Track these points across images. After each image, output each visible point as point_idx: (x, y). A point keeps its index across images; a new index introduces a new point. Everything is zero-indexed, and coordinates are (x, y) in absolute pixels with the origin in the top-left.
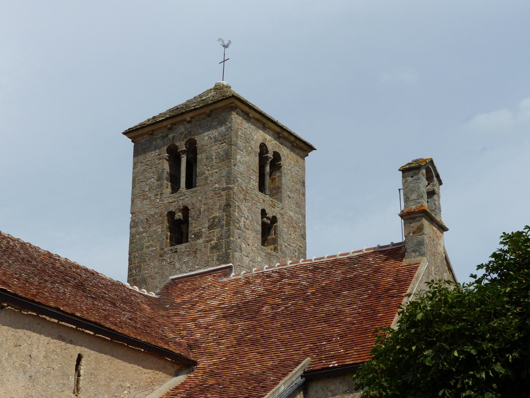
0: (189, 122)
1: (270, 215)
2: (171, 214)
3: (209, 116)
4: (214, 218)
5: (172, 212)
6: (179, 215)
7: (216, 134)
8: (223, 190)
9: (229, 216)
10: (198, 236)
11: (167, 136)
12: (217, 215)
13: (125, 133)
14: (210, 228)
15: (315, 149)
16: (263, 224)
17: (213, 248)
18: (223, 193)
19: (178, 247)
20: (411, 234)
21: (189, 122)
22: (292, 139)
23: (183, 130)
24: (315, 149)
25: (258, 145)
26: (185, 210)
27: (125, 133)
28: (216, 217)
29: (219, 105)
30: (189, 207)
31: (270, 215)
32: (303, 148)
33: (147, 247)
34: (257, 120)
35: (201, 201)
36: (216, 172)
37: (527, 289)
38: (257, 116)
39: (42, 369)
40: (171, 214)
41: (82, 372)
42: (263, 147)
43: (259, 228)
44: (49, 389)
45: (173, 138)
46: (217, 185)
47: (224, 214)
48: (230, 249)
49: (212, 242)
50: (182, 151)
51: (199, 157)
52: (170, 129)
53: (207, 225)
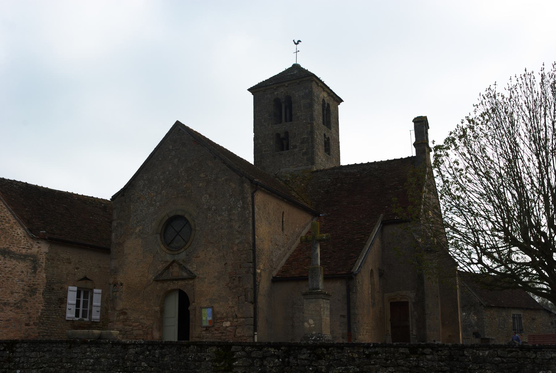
0: (287, 86)
1: (327, 137)
3: (298, 84)
6: (282, 136)
8: (309, 124)
9: (313, 138)
10: (295, 147)
11: (273, 93)
12: (306, 136)
13: (249, 90)
14: (302, 143)
17: (304, 154)
18: (309, 125)
19: (283, 152)
21: (287, 86)
22: (329, 92)
26: (287, 133)
27: (249, 90)
29: (304, 79)
31: (327, 137)
32: (340, 100)
33: (265, 151)
34: (321, 87)
37: (555, 149)
38: (322, 85)
40: (278, 135)
42: (323, 100)
43: (323, 143)
45: (277, 94)
51: (293, 105)
52: (275, 89)
53: (300, 141)
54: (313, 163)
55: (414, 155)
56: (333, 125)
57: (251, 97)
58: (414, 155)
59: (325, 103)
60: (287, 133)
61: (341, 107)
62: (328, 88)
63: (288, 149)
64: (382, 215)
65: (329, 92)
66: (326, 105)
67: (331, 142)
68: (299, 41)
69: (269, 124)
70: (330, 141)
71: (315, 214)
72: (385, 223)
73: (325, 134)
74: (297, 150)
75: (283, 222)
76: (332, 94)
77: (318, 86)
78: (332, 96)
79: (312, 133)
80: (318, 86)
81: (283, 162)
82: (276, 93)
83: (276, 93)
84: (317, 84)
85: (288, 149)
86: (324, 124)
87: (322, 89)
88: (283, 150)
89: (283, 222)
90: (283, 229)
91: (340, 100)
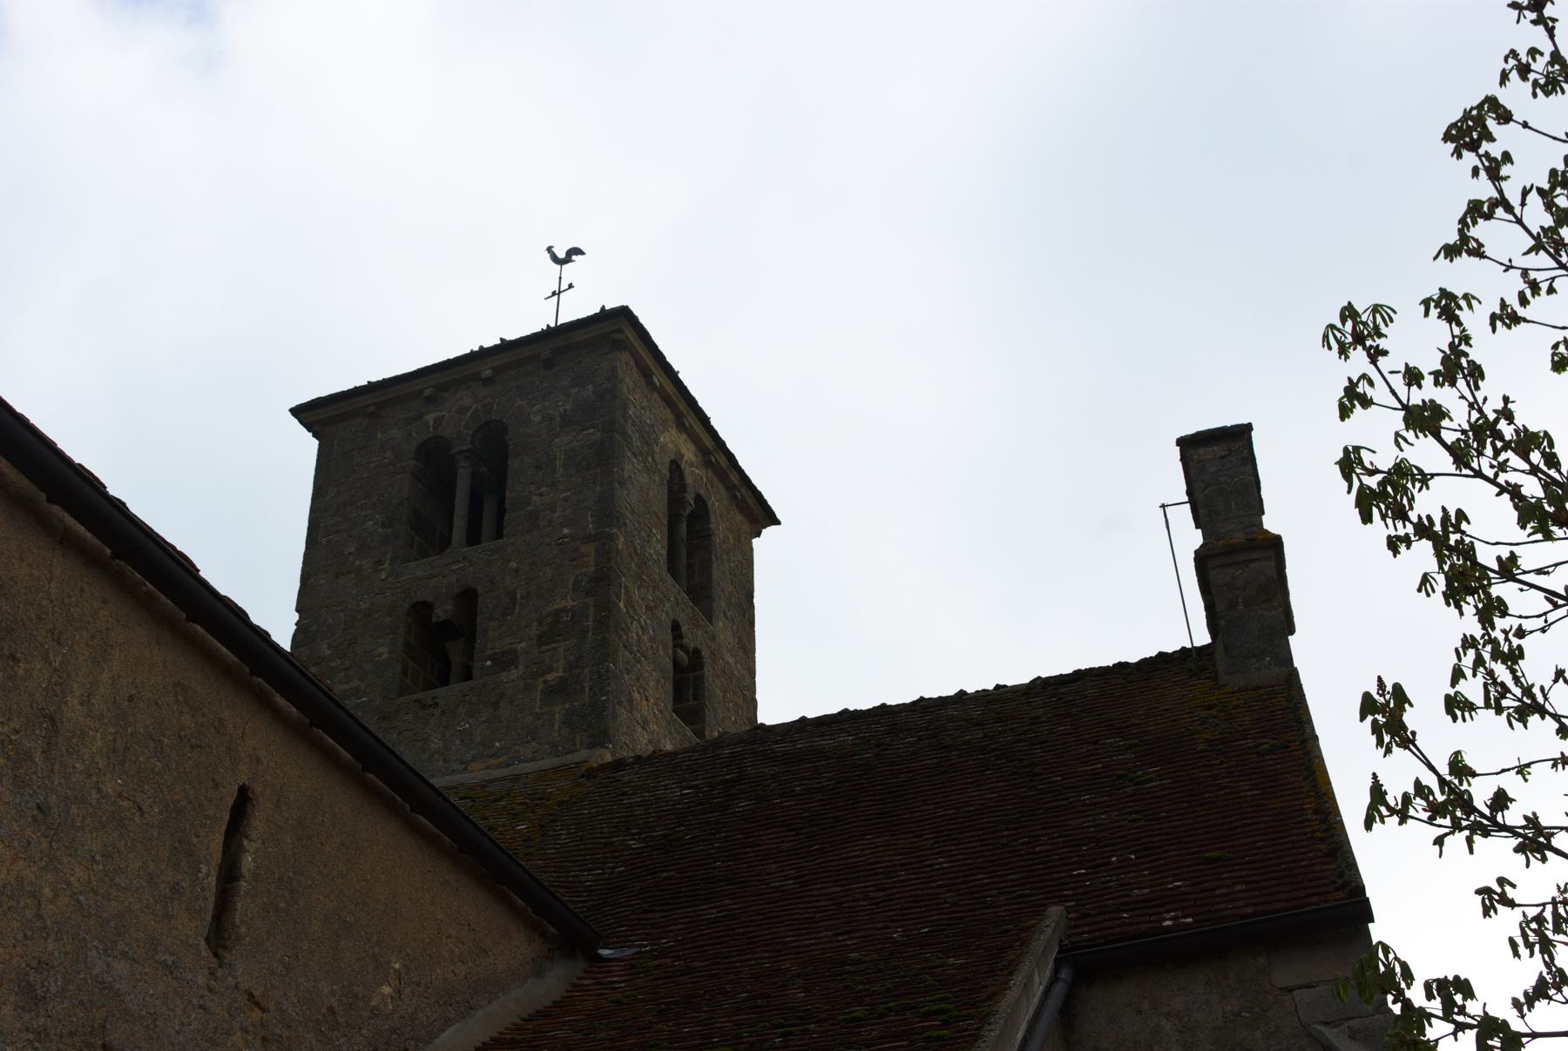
0: (489, 381)
2: (421, 610)
3: (548, 364)
4: (557, 612)
5: (424, 603)
6: (443, 611)
7: (568, 407)
8: (588, 539)
10: (506, 661)
12: (569, 603)
13: (297, 412)
14: (544, 638)
15: (778, 523)
16: (676, 664)
17: (552, 692)
18: (589, 549)
19: (441, 692)
20: (1241, 607)
21: (489, 381)
22: (709, 443)
23: (467, 401)
24: (778, 523)
25: (667, 460)
26: (468, 598)
28: (564, 610)
30: (480, 589)
32: (764, 516)
35: (517, 571)
36: (565, 499)
39: (94, 795)
40: (421, 610)
41: (248, 862)
42: (675, 466)
44: (113, 892)
45: (439, 421)
46: (566, 531)
47: (591, 601)
48: (607, 693)
49: (549, 677)
50: (461, 452)
51: (513, 463)
53: (534, 631)
54: (600, 738)
55: (1203, 638)
56: (720, 604)
57: (302, 450)
58: (1203, 638)
59: (683, 488)
60: (468, 598)
61: (765, 546)
62: (704, 420)
63: (468, 675)
64: (1055, 911)
65: (709, 443)
66: (690, 497)
67: (714, 684)
68: (577, 251)
69: (380, 562)
70: (708, 671)
71: (566, 932)
72: (1087, 967)
73: (676, 627)
74: (514, 673)
75: (229, 874)
76: (723, 462)
77: (650, 383)
78: (721, 474)
79: (602, 583)
80: (650, 383)
81: (436, 743)
82: (430, 417)
83: (430, 417)
84: (647, 375)
85: (468, 675)
86: (673, 569)
87: (669, 415)
88: (444, 681)
89: (229, 874)
90: (219, 934)
91: (764, 516)
